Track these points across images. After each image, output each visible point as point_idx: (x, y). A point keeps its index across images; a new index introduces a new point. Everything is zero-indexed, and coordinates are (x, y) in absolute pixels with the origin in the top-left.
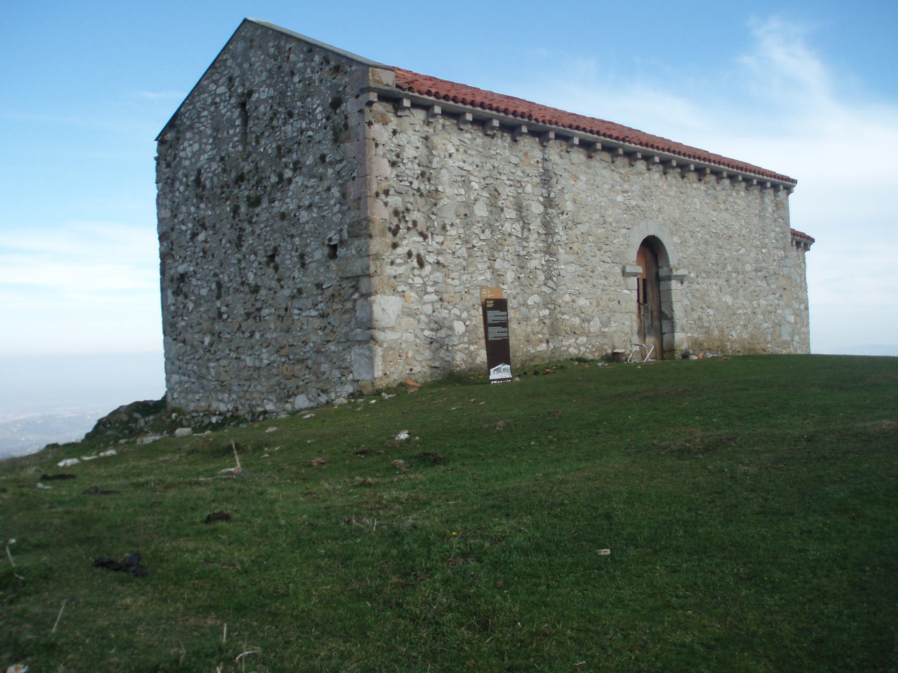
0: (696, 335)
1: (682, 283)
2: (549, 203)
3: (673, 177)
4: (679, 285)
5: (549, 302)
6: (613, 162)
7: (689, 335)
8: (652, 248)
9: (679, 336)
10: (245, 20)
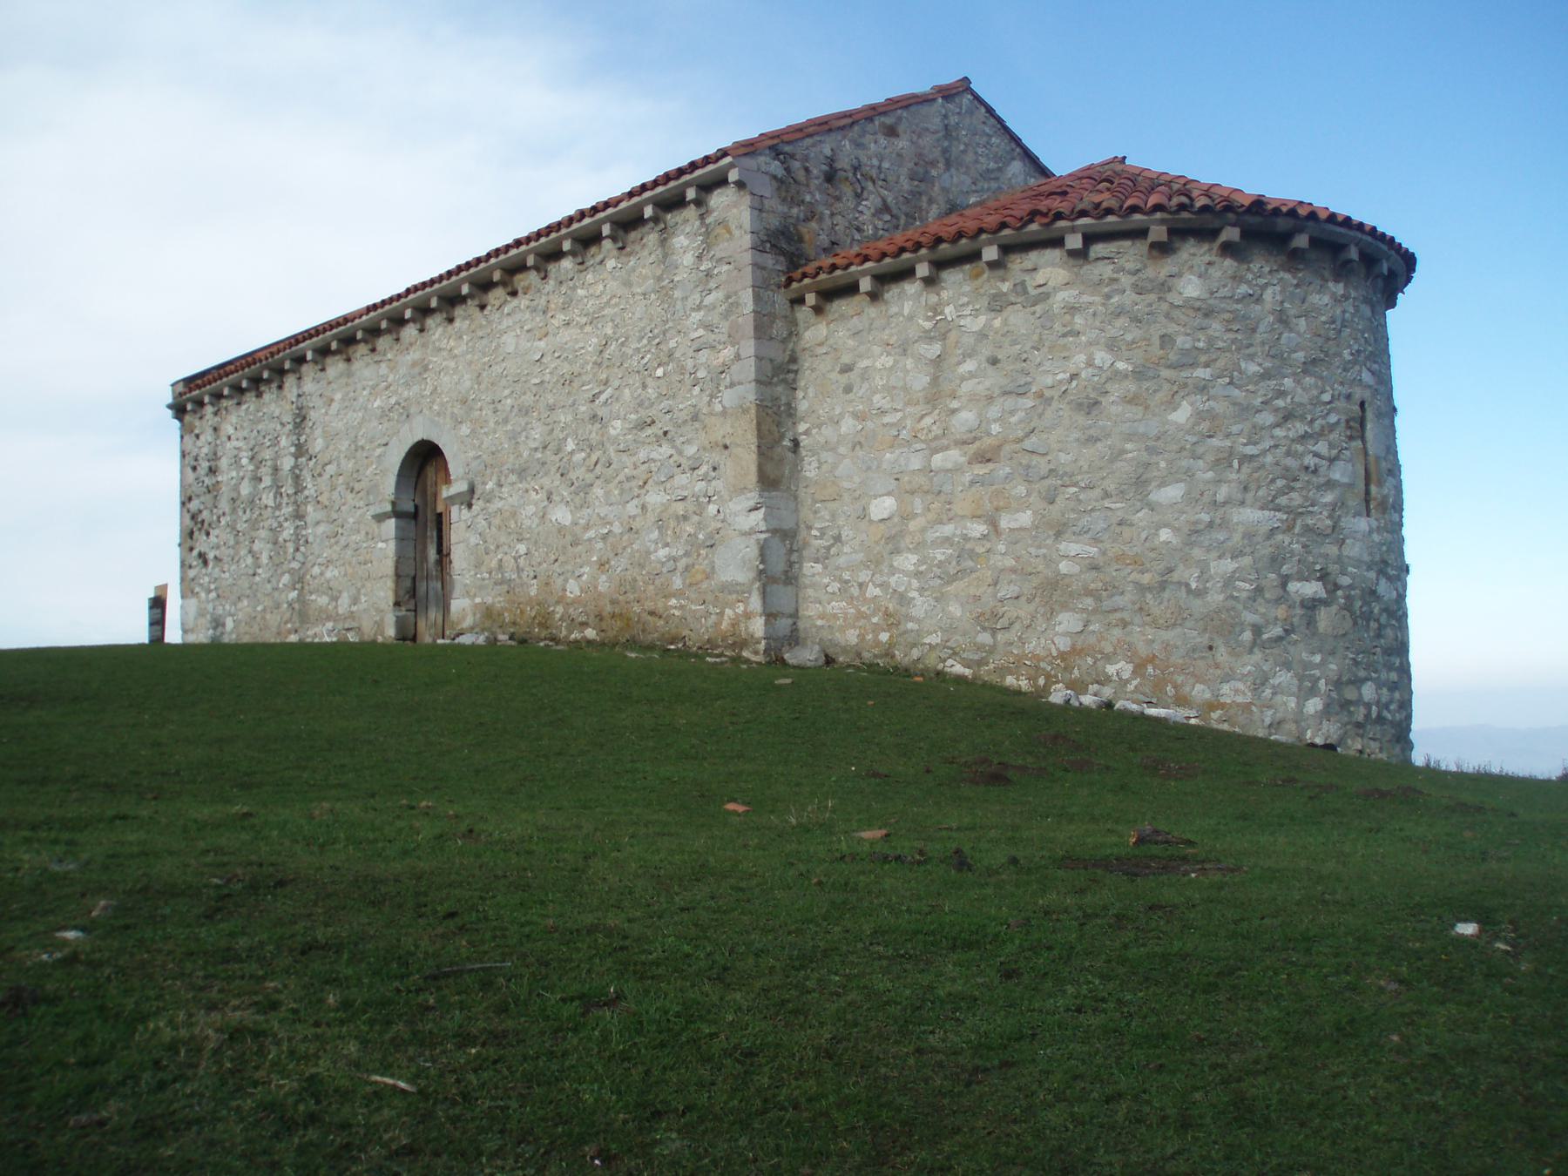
0: (489, 600)
1: (470, 506)
2: (300, 450)
3: (335, 367)
4: (465, 511)
5: (299, 580)
6: (373, 350)
7: (478, 600)
8: (424, 459)
9: (458, 604)
10: (964, 85)
